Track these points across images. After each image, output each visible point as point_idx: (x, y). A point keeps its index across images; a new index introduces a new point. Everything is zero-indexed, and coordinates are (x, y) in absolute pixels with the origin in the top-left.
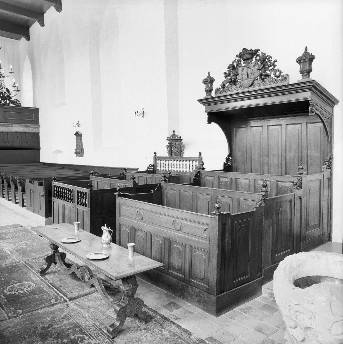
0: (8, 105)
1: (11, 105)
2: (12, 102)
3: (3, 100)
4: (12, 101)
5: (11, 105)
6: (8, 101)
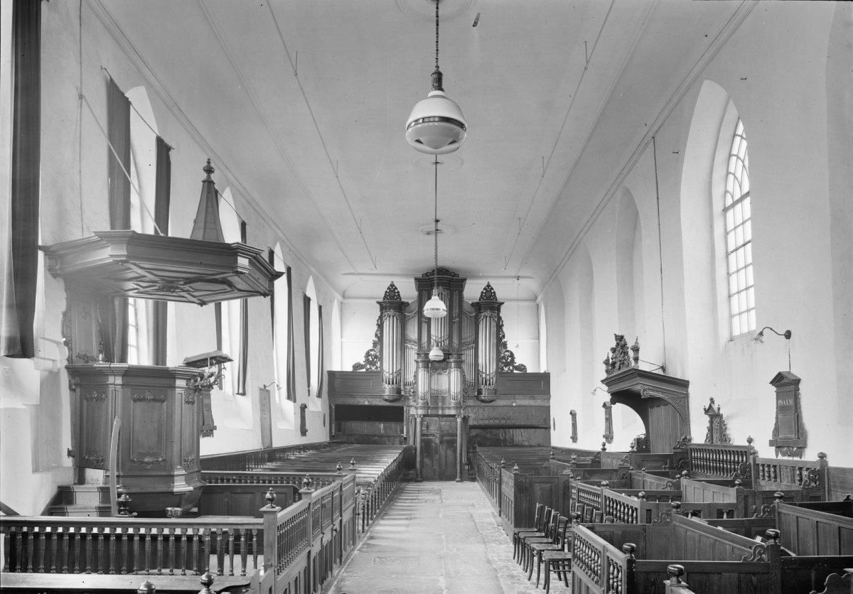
0: (512, 371)
1: (515, 371)
3: (506, 366)
4: (517, 366)
5: (515, 371)
6: (511, 368)
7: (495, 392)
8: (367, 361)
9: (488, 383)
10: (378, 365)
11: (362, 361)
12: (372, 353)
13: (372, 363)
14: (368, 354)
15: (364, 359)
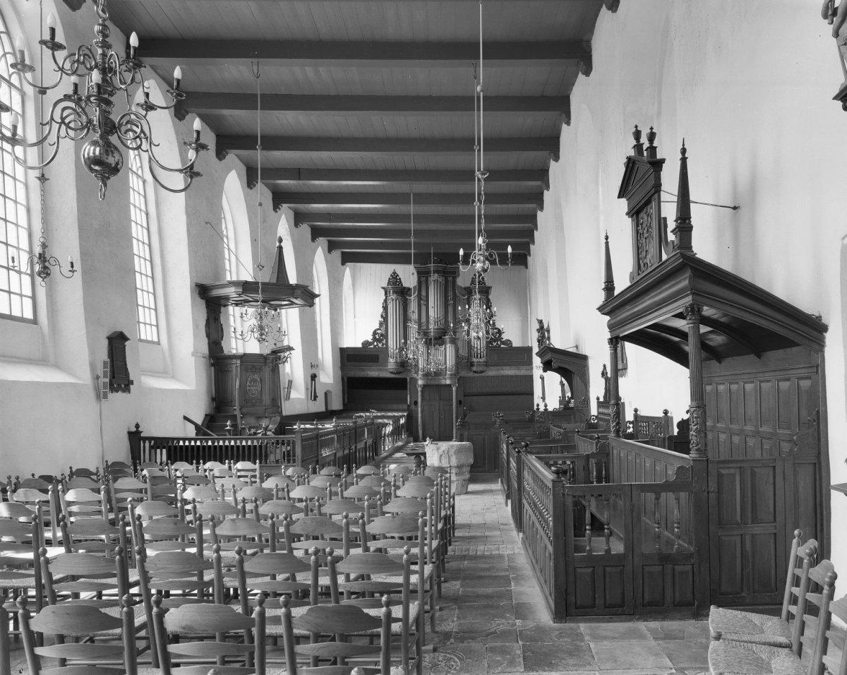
0: (500, 346)
1: (502, 346)
2: (503, 343)
5: (502, 346)
7: (487, 364)
8: (374, 339)
9: (479, 356)
10: (384, 342)
11: (370, 338)
12: (379, 331)
13: (379, 341)
14: (375, 333)
15: (372, 337)
